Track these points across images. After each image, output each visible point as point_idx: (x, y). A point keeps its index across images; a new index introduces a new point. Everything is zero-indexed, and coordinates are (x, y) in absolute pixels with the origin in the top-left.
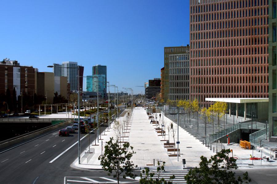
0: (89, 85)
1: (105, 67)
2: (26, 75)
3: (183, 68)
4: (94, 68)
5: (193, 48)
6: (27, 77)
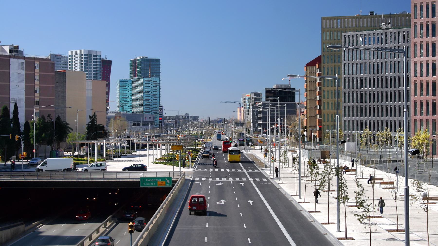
0: (125, 99)
1: (157, 61)
2: (37, 77)
3: (374, 61)
4: (134, 63)
5: (418, 16)
6: (39, 80)
